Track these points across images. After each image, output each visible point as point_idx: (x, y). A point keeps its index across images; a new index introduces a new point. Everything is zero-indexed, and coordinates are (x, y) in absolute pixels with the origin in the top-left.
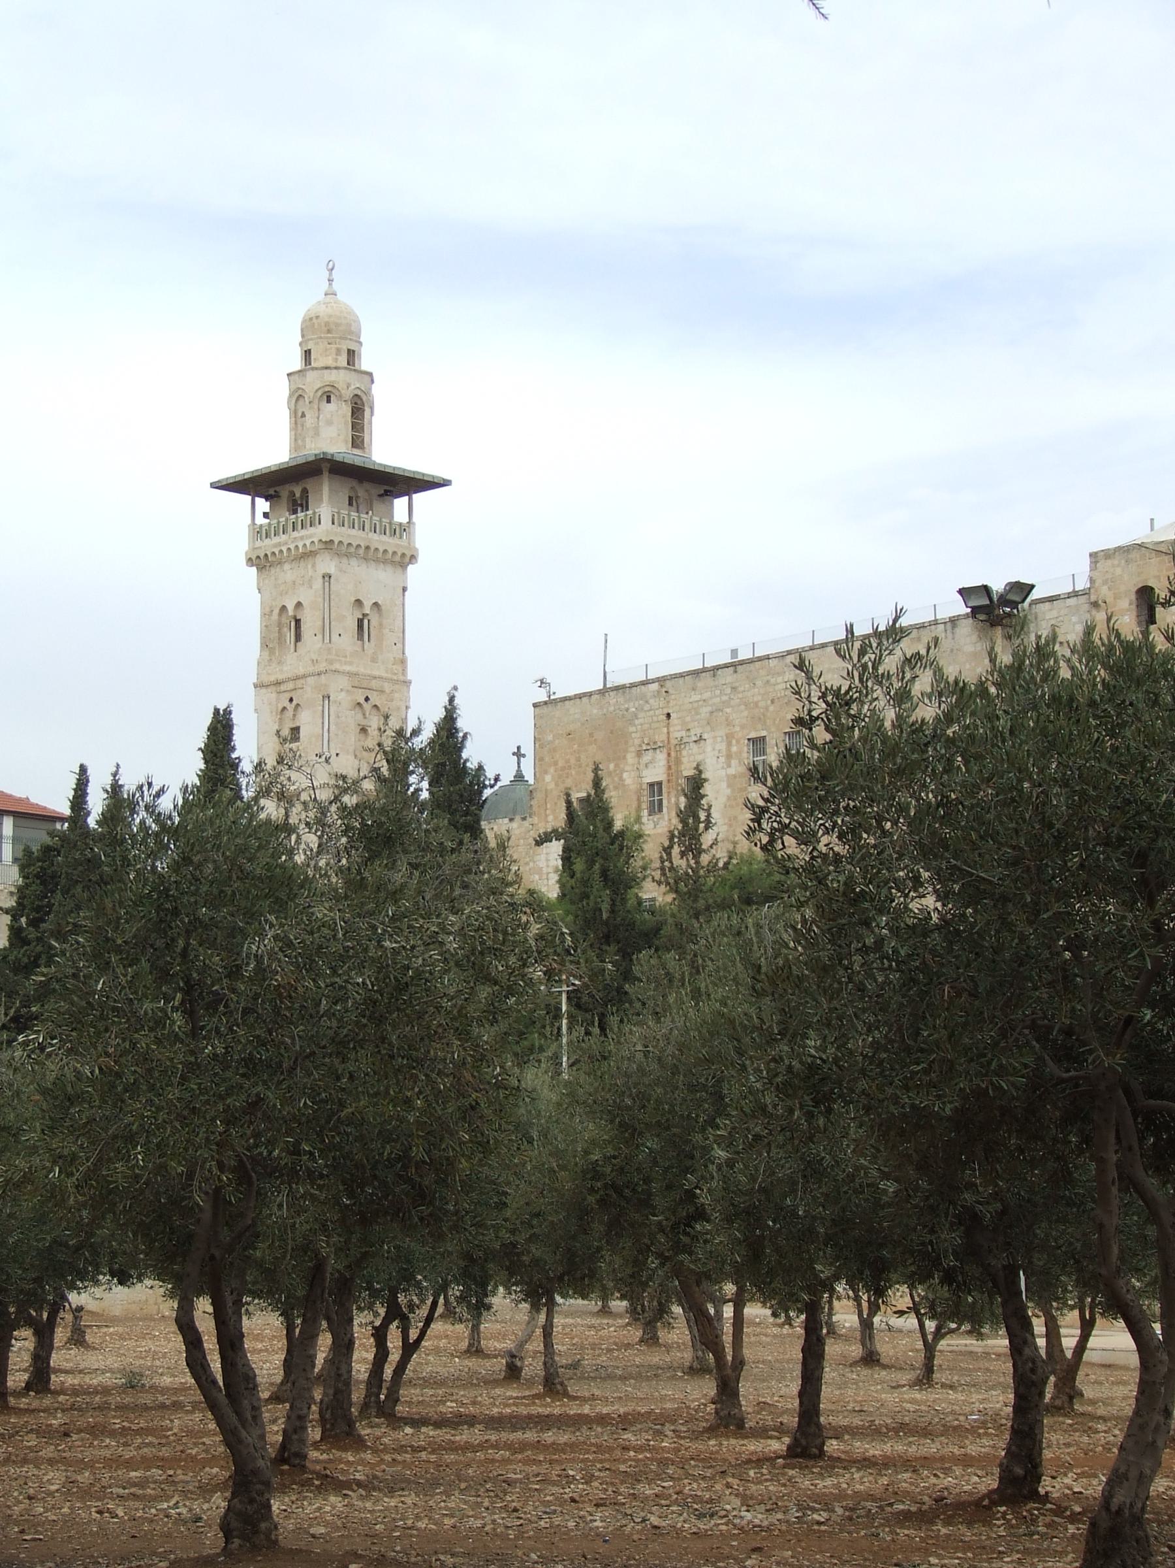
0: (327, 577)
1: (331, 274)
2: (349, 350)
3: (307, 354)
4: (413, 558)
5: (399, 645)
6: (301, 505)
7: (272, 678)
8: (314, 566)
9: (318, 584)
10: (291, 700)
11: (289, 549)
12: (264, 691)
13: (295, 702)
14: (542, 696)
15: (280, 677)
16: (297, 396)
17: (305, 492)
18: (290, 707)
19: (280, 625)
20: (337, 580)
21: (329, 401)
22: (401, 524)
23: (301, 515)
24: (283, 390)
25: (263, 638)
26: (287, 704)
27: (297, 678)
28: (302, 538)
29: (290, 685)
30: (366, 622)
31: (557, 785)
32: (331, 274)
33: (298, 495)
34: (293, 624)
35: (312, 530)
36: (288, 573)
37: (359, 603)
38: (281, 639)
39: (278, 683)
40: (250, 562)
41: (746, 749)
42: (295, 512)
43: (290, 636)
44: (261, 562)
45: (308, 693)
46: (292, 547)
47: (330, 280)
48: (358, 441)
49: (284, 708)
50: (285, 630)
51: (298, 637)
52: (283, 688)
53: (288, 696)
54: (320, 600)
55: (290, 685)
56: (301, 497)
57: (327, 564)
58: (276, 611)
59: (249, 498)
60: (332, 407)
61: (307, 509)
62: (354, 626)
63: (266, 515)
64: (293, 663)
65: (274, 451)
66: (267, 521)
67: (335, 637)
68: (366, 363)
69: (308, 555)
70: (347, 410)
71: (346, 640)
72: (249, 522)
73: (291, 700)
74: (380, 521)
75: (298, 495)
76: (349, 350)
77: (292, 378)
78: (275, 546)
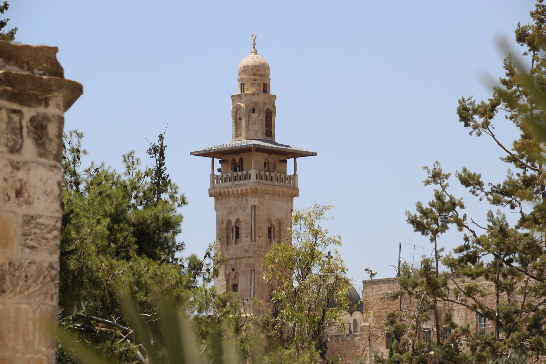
0: (254, 207)
1: (254, 41)
2: (264, 84)
3: (242, 85)
4: (297, 195)
5: (289, 240)
6: (239, 166)
8: (246, 200)
9: (248, 210)
10: (233, 270)
11: (233, 190)
13: (235, 271)
14: (367, 277)
16: (236, 112)
17: (241, 160)
18: (233, 273)
19: (228, 228)
20: (259, 208)
21: (254, 112)
22: (290, 176)
23: (240, 173)
24: (229, 107)
25: (217, 235)
26: (231, 271)
27: (237, 258)
28: (240, 185)
29: (233, 262)
30: (272, 229)
31: (375, 324)
32: (254, 41)
33: (237, 161)
34: (234, 230)
35: (246, 181)
36: (232, 202)
37: (269, 220)
38: (228, 238)
40: (211, 195)
41: (475, 317)
42: (235, 170)
43: (233, 236)
44: (217, 195)
45: (242, 267)
46: (235, 189)
47: (254, 45)
48: (269, 133)
49: (229, 274)
50: (230, 231)
51: (237, 236)
52: (229, 263)
53: (232, 267)
54: (250, 218)
55: (233, 262)
56: (239, 162)
57: (253, 201)
58: (225, 222)
59: (211, 159)
60: (255, 115)
61: (242, 170)
62: (266, 231)
63: (219, 170)
64: (234, 250)
65: (226, 138)
66: (220, 174)
67: (257, 238)
68: (272, 92)
69: (243, 195)
70: (263, 117)
71: (262, 240)
72: (211, 173)
73: (233, 270)
74: (280, 175)
75: (237, 161)
76: (264, 84)
77: (234, 97)
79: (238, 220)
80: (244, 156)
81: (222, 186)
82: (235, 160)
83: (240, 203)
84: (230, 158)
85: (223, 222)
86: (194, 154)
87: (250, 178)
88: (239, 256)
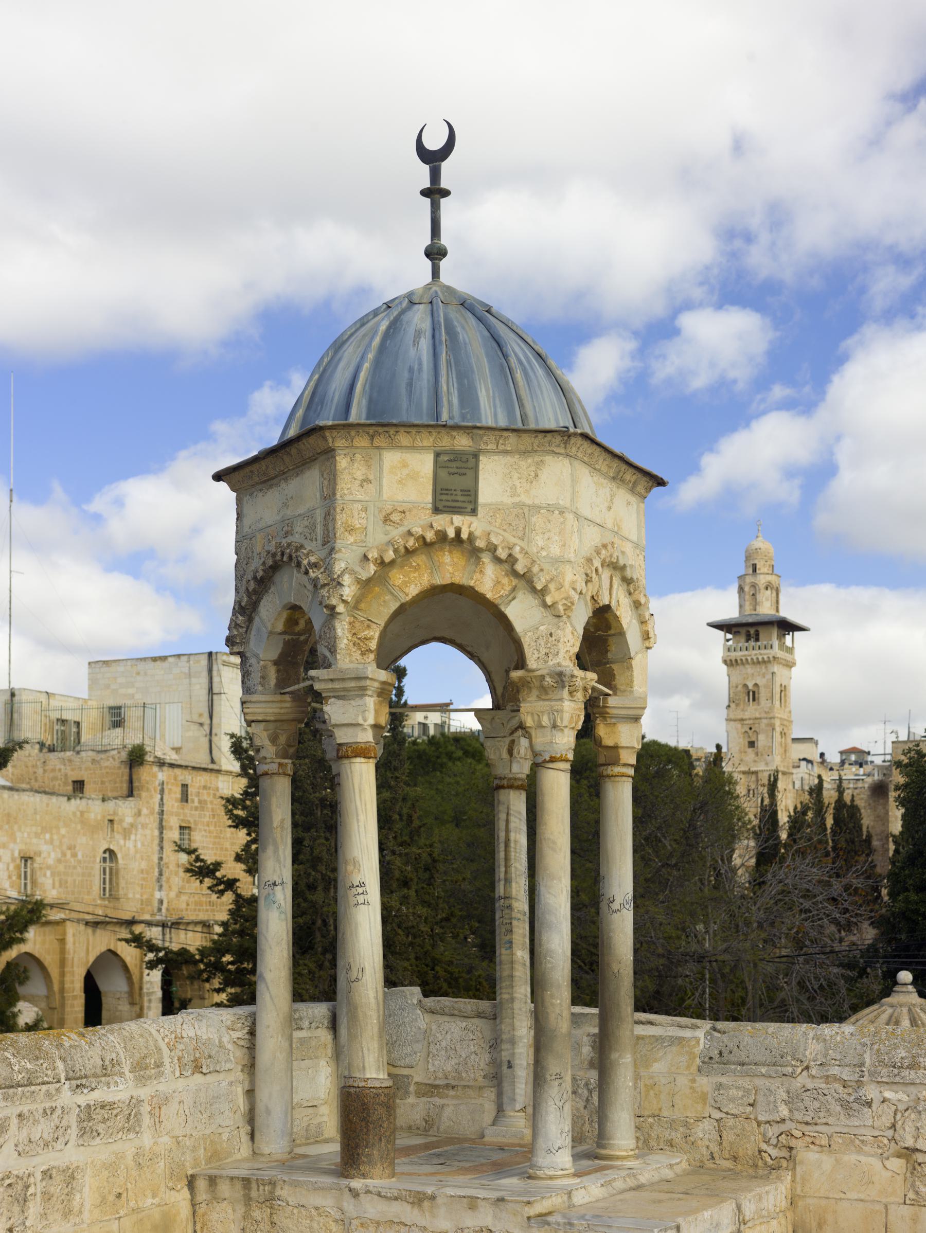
1: (435, 175)
7: (739, 717)
27: (756, 719)
29: (751, 722)
32: (435, 175)
39: (742, 720)
44: (730, 663)
46: (755, 658)
78: (745, 656)
79: (756, 685)
80: (760, 629)
81: (733, 655)
83: (764, 670)
84: (743, 630)
85: (737, 687)
86: (711, 625)
88: (758, 716)
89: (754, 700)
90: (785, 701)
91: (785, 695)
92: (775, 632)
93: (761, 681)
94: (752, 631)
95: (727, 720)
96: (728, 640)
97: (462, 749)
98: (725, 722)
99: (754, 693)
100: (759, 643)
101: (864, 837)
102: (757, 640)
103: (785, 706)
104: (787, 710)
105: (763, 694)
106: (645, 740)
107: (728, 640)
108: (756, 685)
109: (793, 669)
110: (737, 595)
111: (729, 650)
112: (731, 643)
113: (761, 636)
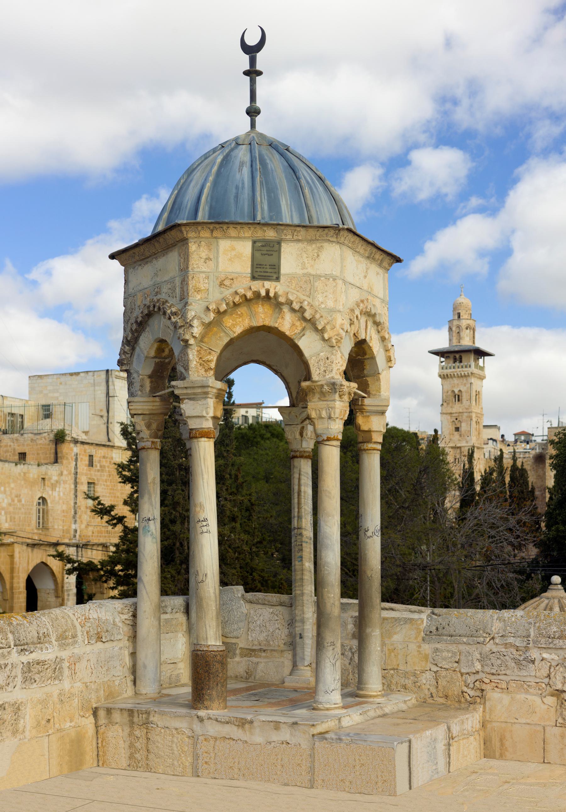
7: (449, 412)
10: (456, 419)
12: (444, 415)
15: (452, 412)
27: (460, 413)
29: (457, 415)
34: (457, 396)
39: (451, 413)
44: (443, 377)
46: (459, 373)
55: (457, 415)
60: (468, 331)
70: (472, 332)
79: (460, 391)
81: (446, 372)
82: (455, 356)
84: (452, 356)
85: (448, 392)
87: (470, 367)
88: (461, 411)
89: (459, 400)
90: (479, 402)
91: (479, 398)
92: (472, 356)
93: (463, 389)
94: (457, 356)
95: (441, 413)
96: (442, 362)
97: (270, 432)
98: (440, 415)
99: (459, 396)
100: (462, 364)
101: (530, 489)
102: (461, 362)
103: (479, 405)
104: (480, 407)
105: (464, 397)
106: (389, 426)
107: (442, 362)
108: (460, 391)
109: (484, 380)
110: (448, 333)
111: (442, 368)
112: (444, 364)
113: (463, 359)
